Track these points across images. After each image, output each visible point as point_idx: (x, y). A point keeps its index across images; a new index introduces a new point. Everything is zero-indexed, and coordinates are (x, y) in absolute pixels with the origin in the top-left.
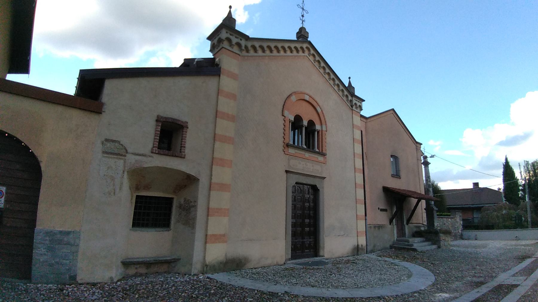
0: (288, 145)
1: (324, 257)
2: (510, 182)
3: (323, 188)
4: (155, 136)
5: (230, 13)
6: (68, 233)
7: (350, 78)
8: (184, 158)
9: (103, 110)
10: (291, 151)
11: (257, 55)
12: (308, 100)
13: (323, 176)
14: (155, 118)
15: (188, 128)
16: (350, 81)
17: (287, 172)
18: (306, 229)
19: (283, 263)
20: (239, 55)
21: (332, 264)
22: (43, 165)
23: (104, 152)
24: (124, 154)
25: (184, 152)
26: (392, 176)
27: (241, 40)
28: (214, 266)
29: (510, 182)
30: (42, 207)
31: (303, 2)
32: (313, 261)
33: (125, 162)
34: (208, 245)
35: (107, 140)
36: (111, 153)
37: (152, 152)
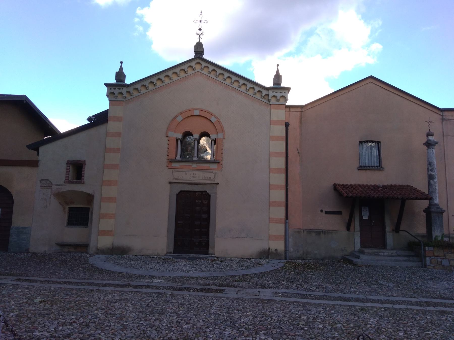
0: (171, 161)
1: (214, 255)
2: (423, 256)
3: (216, 193)
4: (66, 173)
5: (121, 68)
6: (25, 228)
7: (278, 65)
8: (84, 183)
9: (39, 164)
10: (174, 165)
12: (198, 114)
13: (216, 182)
14: (66, 162)
15: (85, 164)
16: (278, 69)
17: (170, 183)
18: (195, 229)
19: (164, 254)
20: (124, 101)
22: (14, 197)
23: (41, 186)
24: (51, 186)
25: (83, 180)
26: (358, 170)
29: (423, 256)
30: (14, 216)
31: (201, 13)
32: (198, 257)
33: (51, 190)
35: (42, 180)
36: (45, 186)
37: (65, 183)
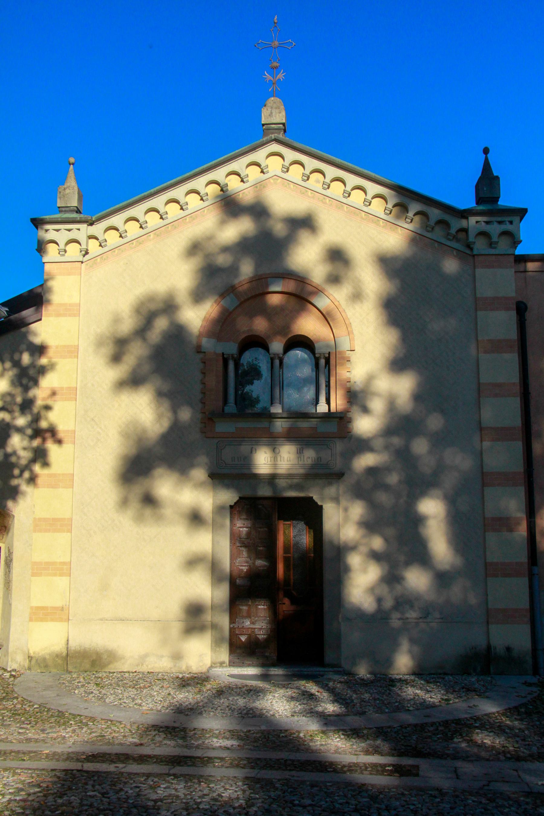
7: (486, 151)
11: (494, 253)
21: (502, 725)
27: (511, 223)
28: (44, 659)
34: (70, 561)
